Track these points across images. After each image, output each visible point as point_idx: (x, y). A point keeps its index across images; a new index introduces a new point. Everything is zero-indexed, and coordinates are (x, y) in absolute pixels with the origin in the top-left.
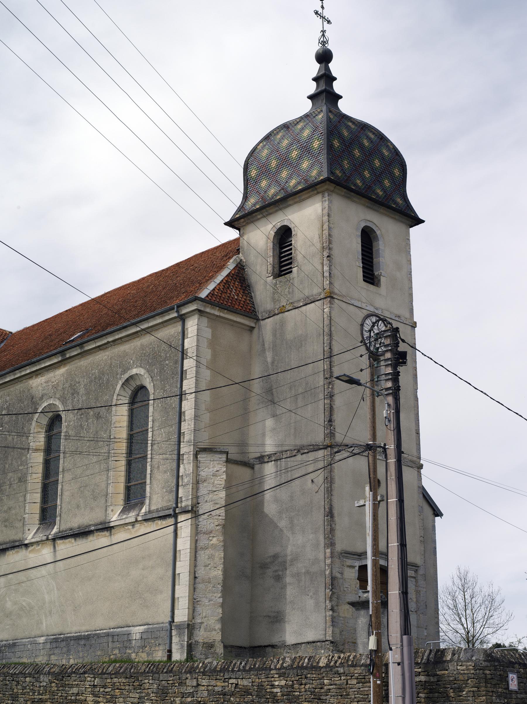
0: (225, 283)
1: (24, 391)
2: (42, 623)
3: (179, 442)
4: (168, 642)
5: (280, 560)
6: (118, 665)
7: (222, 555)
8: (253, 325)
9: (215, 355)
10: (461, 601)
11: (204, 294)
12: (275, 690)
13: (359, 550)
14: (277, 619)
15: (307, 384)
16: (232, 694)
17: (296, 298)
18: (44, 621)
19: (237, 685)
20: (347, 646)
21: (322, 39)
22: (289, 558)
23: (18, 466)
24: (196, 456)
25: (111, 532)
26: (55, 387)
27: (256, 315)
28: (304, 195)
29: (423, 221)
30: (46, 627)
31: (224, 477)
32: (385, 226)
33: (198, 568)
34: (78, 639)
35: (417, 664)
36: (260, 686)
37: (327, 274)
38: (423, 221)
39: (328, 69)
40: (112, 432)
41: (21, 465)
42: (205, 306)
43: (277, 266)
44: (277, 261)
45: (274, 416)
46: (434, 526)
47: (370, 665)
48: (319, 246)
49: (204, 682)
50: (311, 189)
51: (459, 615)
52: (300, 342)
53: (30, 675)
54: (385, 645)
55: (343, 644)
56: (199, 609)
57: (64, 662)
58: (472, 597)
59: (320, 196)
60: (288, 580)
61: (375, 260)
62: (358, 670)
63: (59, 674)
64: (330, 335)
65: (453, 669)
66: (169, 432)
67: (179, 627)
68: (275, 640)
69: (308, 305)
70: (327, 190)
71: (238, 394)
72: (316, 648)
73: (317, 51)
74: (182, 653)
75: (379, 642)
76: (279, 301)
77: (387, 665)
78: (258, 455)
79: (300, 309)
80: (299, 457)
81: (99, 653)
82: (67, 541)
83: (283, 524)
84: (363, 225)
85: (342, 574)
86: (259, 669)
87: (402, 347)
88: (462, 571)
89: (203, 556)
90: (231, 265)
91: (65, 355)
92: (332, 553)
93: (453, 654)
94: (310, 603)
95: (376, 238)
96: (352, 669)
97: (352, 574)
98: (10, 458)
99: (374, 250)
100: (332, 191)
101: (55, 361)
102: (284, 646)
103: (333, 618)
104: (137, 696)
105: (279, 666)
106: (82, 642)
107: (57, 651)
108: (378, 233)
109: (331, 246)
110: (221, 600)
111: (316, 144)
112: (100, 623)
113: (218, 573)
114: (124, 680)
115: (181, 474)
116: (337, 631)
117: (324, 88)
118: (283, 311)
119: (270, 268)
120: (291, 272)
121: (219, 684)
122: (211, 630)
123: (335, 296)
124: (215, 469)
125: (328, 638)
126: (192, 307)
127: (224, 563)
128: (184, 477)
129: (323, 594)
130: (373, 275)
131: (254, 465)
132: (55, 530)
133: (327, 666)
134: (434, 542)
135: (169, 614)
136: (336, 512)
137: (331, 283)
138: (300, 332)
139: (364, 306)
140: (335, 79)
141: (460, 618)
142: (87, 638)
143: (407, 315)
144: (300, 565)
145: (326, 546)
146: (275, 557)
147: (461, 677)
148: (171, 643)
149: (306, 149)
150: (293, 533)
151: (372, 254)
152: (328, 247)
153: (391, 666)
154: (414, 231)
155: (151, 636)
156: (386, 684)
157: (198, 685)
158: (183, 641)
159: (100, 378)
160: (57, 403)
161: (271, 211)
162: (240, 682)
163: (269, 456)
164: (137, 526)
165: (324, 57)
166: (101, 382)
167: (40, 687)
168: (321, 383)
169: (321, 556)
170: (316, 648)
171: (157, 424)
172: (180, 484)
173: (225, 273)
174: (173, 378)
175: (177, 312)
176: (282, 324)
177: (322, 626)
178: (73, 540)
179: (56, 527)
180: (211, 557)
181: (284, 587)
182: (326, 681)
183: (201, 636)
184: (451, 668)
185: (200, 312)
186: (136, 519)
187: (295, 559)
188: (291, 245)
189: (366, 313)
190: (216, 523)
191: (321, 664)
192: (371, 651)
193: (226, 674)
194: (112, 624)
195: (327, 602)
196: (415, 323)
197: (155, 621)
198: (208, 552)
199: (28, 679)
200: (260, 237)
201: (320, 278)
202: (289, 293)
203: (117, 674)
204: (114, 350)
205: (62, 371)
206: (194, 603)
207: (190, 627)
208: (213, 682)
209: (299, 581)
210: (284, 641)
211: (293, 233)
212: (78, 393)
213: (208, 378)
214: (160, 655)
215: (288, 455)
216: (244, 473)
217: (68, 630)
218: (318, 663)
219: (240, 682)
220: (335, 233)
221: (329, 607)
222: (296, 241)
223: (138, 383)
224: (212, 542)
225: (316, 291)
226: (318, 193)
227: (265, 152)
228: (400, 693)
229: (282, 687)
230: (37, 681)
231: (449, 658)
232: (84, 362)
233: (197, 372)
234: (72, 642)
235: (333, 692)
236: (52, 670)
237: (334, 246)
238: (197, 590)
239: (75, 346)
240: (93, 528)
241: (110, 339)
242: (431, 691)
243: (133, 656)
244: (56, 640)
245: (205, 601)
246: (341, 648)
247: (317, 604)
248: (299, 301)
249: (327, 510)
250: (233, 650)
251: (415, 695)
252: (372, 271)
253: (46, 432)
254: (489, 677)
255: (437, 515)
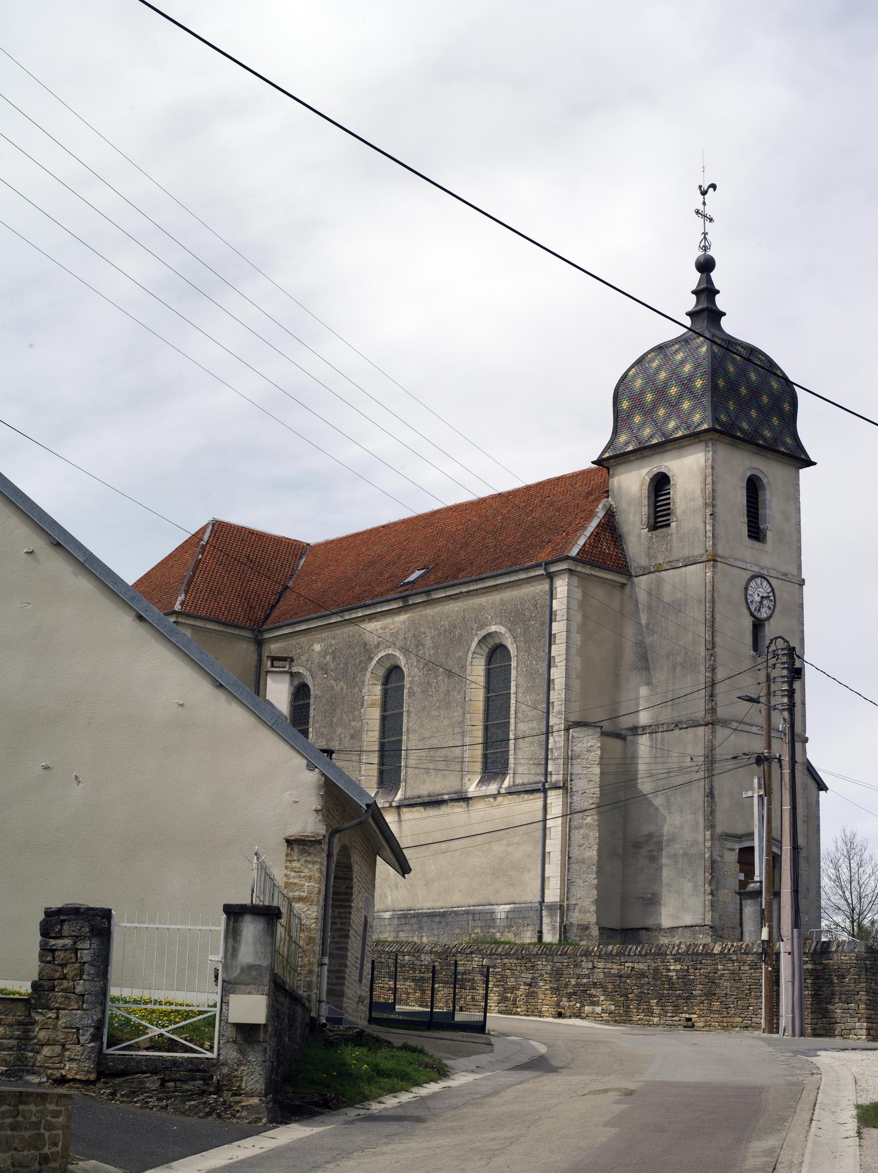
0: (595, 535)
1: (353, 636)
2: (386, 897)
3: (548, 713)
4: (538, 922)
5: (655, 839)
6: (507, 946)
7: (597, 835)
8: (625, 581)
9: (585, 617)
10: (845, 870)
11: (574, 552)
12: (671, 974)
13: (740, 830)
14: (652, 901)
15: (686, 653)
16: (628, 977)
17: (674, 557)
18: (389, 894)
19: (633, 968)
20: (726, 931)
21: (703, 244)
22: (665, 838)
23: (350, 722)
24: (567, 729)
25: (468, 804)
26: (395, 635)
27: (628, 571)
28: (685, 442)
29: (815, 464)
30: (392, 901)
31: (599, 752)
32: (772, 472)
33: (572, 848)
34: (431, 915)
35: (805, 953)
36: (656, 970)
37: (709, 534)
38: (815, 464)
39: (709, 281)
40: (468, 694)
41: (354, 720)
42: (576, 565)
43: (652, 516)
44: (652, 510)
45: (649, 683)
46: (818, 802)
47: (761, 953)
48: (700, 501)
49: (601, 965)
50: (693, 438)
51: (842, 887)
52: (678, 607)
53: (409, 953)
54: (775, 936)
55: (723, 929)
56: (573, 890)
57: (415, 939)
58: (860, 866)
59: (702, 445)
60: (664, 861)
61: (760, 511)
62: (750, 958)
63: (442, 953)
64: (713, 602)
65: (840, 959)
66: (536, 700)
67: (551, 907)
68: (649, 923)
69: (689, 567)
70: (711, 439)
71: (612, 661)
72: (694, 933)
73: (698, 259)
74: (554, 934)
75: (770, 933)
76: (656, 558)
77: (778, 954)
78: (631, 725)
79: (679, 570)
80: (677, 732)
81: (457, 931)
82: (415, 809)
83: (658, 801)
84: (748, 474)
85: (722, 857)
86: (655, 954)
87: (797, 665)
88: (848, 833)
89: (577, 836)
90: (600, 513)
91: (407, 601)
92: (712, 836)
93: (838, 946)
94: (688, 886)
95: (763, 487)
96: (745, 957)
97: (732, 858)
98: (338, 711)
99: (760, 500)
100: (717, 440)
101: (396, 606)
102: (659, 929)
103: (712, 903)
104: (530, 976)
105: (674, 952)
106: (437, 919)
107: (406, 928)
108: (765, 481)
109: (715, 502)
110: (596, 882)
111: (699, 383)
112: (457, 900)
113: (593, 853)
114: (515, 961)
115: (550, 747)
116: (716, 915)
117: (705, 306)
118: (659, 569)
119: (645, 519)
120: (669, 525)
121: (615, 967)
122: (585, 912)
123: (718, 559)
124: (589, 744)
125: (707, 923)
126: (563, 566)
127: (599, 844)
128: (554, 751)
129: (702, 877)
130: (758, 528)
131: (625, 736)
132: (399, 796)
133: (721, 953)
134: (818, 818)
135: (539, 894)
136: (716, 793)
137: (714, 545)
138: (679, 595)
139: (748, 566)
140: (718, 292)
141: (844, 892)
142: (443, 915)
143: (795, 573)
144: (677, 846)
145: (706, 828)
146: (650, 836)
147: (844, 966)
148: (541, 923)
149: (686, 385)
150: (670, 813)
151: (757, 504)
152: (712, 502)
153: (782, 955)
154: (804, 472)
155: (518, 915)
156: (777, 970)
157: (594, 967)
158: (556, 922)
159: (451, 632)
160: (398, 653)
161: (646, 454)
162: (636, 965)
163: (644, 728)
164: (500, 799)
165: (706, 266)
166: (453, 637)
167: (421, 965)
168: (703, 654)
169: (701, 839)
170: (694, 933)
171: (521, 690)
172: (550, 757)
173: (594, 523)
174: (539, 641)
175: (545, 569)
176: (659, 583)
177: (701, 910)
178: (422, 809)
179: (400, 792)
180: (585, 837)
181: (660, 868)
182: (719, 967)
183: (575, 917)
184: (835, 958)
185: (570, 571)
186: (499, 792)
187: (672, 839)
188: (669, 493)
189: (750, 574)
190: (591, 801)
191: (715, 952)
192: (763, 941)
193: (622, 958)
194: (472, 901)
195: (707, 886)
196: (804, 580)
197: (523, 900)
198: (582, 831)
199: (407, 958)
200: (632, 482)
201: (702, 538)
202: (667, 550)
203: (507, 955)
204: (467, 602)
205: (403, 617)
206: (567, 884)
207: (562, 909)
208: (609, 965)
209: (676, 863)
210: (660, 925)
211: (672, 482)
212: (424, 646)
213: (579, 643)
214: (528, 937)
215: (665, 729)
216: (617, 744)
217: (419, 906)
218: (713, 950)
219: (636, 965)
220: (719, 487)
221: (709, 891)
222: (675, 492)
223: (497, 641)
224: (586, 821)
225: (698, 551)
226: (701, 441)
227: (639, 383)
228: (790, 979)
229: (677, 971)
230: (417, 959)
231: (833, 949)
232: (431, 612)
233: (568, 637)
234: (425, 919)
235: (727, 976)
236: (434, 950)
237: (718, 502)
238: (571, 871)
239: (421, 593)
240: (446, 797)
241: (464, 590)
242: (817, 978)
243: (498, 935)
244: (405, 916)
245: (580, 882)
246: (720, 933)
247: (695, 888)
248: (678, 560)
249: (707, 790)
250: (608, 933)
251: (803, 981)
252: (758, 524)
253: (383, 684)
254: (869, 966)
255: (822, 790)
